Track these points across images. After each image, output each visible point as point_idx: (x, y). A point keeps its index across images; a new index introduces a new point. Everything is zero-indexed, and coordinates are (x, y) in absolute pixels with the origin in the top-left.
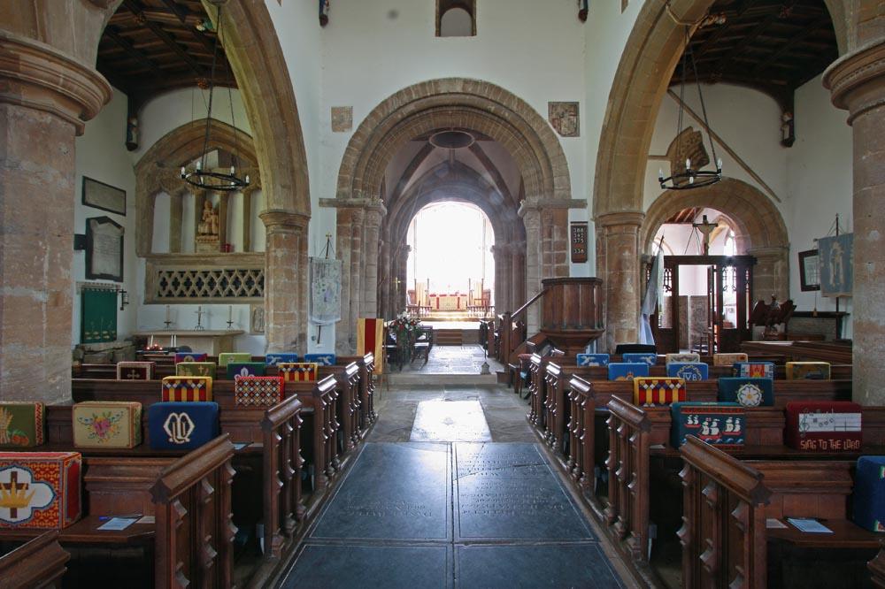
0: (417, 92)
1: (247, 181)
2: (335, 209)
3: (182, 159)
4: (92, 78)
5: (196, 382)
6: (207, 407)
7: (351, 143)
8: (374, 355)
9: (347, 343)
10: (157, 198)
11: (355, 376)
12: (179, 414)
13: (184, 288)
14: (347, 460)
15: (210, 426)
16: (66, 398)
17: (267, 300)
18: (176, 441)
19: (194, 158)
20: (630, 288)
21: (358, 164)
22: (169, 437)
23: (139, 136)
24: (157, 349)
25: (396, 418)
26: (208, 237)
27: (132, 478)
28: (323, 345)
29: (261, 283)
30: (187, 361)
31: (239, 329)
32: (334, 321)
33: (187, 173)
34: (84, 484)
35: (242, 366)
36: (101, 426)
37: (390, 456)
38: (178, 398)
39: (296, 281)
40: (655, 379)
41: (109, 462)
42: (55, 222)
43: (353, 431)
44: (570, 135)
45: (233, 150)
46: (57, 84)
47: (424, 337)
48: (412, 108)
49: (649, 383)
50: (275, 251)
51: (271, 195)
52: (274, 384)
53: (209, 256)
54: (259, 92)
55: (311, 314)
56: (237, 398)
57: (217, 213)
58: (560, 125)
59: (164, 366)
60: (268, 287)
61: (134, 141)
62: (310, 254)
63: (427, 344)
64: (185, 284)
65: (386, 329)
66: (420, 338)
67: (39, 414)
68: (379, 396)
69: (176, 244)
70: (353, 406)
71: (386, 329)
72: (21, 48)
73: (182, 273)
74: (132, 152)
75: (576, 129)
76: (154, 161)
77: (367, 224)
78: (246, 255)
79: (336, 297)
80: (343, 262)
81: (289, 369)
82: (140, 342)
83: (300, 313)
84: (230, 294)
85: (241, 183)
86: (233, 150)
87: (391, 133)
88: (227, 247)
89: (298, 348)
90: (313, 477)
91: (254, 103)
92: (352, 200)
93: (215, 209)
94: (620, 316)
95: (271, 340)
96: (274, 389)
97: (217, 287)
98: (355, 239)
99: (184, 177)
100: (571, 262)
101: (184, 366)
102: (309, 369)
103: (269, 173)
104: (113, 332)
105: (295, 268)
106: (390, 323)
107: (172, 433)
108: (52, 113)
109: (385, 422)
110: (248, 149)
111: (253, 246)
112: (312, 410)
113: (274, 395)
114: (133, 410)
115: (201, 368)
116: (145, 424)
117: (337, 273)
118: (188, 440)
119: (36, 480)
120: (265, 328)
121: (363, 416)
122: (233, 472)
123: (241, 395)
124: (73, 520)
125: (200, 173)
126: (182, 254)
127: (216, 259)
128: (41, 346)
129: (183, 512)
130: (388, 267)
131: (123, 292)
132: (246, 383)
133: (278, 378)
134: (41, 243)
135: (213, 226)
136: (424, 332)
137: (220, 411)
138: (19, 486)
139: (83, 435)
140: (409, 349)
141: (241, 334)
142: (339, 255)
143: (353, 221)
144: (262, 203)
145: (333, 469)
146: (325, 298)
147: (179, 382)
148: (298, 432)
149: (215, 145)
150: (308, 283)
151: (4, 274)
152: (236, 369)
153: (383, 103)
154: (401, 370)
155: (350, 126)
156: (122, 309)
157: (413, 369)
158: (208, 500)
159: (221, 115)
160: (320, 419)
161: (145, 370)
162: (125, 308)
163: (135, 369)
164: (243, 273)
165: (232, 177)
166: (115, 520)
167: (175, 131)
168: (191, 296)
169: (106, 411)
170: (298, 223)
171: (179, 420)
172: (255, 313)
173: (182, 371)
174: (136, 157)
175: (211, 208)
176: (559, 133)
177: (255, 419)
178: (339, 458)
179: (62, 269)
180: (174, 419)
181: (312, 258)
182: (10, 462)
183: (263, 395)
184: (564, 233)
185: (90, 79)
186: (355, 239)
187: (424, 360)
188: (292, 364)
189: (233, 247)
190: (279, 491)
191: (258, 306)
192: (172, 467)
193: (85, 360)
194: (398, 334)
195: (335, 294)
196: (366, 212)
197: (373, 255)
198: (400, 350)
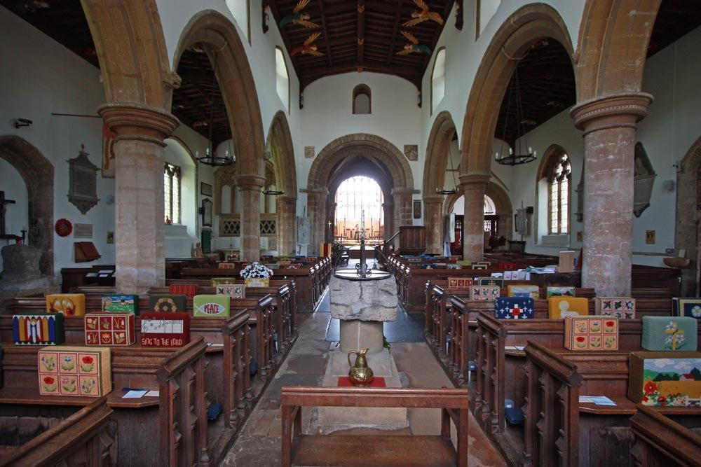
7: (314, 163)
20: (437, 231)
44: (414, 160)
48: (342, 147)
94: (432, 243)
100: (213, 185)
142: (308, 215)
155: (313, 155)
184: (411, 204)
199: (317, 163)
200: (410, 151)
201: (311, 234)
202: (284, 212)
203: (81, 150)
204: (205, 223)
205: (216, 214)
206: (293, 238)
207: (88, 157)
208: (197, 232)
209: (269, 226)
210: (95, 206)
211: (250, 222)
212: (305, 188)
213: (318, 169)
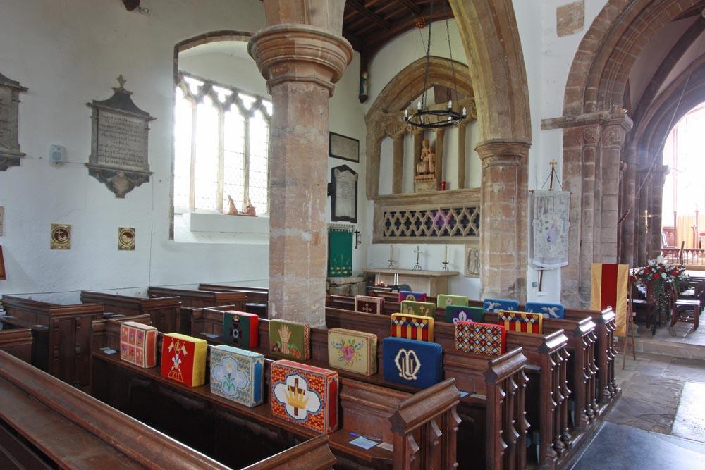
1: (464, 114)
2: (562, 129)
3: (403, 103)
4: (340, 44)
5: (420, 321)
6: (428, 346)
7: (582, 45)
8: (614, 310)
9: (576, 292)
10: (383, 143)
11: (590, 335)
12: (407, 351)
14: (579, 437)
15: (435, 370)
16: (321, 324)
17: (483, 239)
18: (405, 377)
19: (413, 99)
21: (591, 70)
22: (399, 371)
23: (368, 88)
24: (382, 286)
25: (648, 397)
26: (425, 176)
27: (375, 404)
28: (547, 292)
29: (476, 221)
30: (409, 299)
31: (453, 270)
32: (559, 265)
33: (408, 115)
34: (340, 400)
35: (460, 310)
36: (348, 352)
37: (641, 448)
38: (404, 335)
39: (514, 219)
41: (357, 385)
42: (316, 173)
43: (587, 403)
45: (449, 84)
46: (317, 57)
47: (691, 292)
50: (491, 186)
51: (488, 124)
52: (495, 332)
53: (426, 195)
54: (475, 14)
55: (532, 256)
56: (457, 343)
57: (433, 152)
59: (391, 304)
60: (483, 227)
61: (365, 93)
62: (531, 185)
63: (698, 302)
64: (405, 224)
65: (631, 279)
66: (685, 293)
67: (306, 333)
68: (621, 364)
69: (398, 185)
70: (588, 373)
71: (631, 279)
72: (296, 34)
73: (403, 213)
74: (364, 104)
76: (380, 108)
77: (605, 143)
78: (461, 192)
79: (562, 237)
80: (571, 193)
81: (510, 318)
82: (370, 278)
83: (519, 255)
84: (446, 233)
85: (458, 116)
86: (449, 84)
87: (640, 18)
88: (443, 185)
89: (516, 295)
90: (538, 447)
91: (470, 28)
92: (583, 116)
93: (432, 147)
95: (487, 284)
96: (495, 338)
97: (434, 226)
98: (588, 164)
99: (406, 119)
101: (407, 303)
102: (532, 320)
103: (485, 100)
104: (350, 268)
105: (513, 204)
106: (637, 270)
107: (401, 368)
108: (314, 82)
109: (632, 400)
110: (463, 79)
111: (468, 181)
112: (538, 368)
113: (495, 344)
114: (371, 341)
115: (422, 308)
116: (380, 356)
117: (563, 208)
118: (415, 378)
119: (310, 389)
120: (480, 270)
121: (601, 389)
122: (459, 421)
123: (461, 340)
124: (332, 429)
125: (420, 113)
126: (403, 194)
127: (434, 198)
128: (307, 278)
129: (416, 448)
130: (633, 197)
131: (357, 232)
132: (466, 329)
133: (499, 327)
134: (307, 192)
135: (430, 164)
136: (693, 285)
137: (444, 353)
138: (300, 391)
139: (334, 355)
140: (667, 306)
141: (454, 275)
142: (566, 186)
143: (585, 142)
144: (478, 134)
145: (562, 444)
146: (549, 238)
147: (404, 320)
148: (524, 390)
149: (432, 83)
150: (528, 220)
151: (286, 219)
152: (455, 312)
154: (654, 334)
155: (581, 24)
156: (356, 247)
157: (673, 334)
158: (436, 443)
159: (439, 51)
160: (547, 380)
161: (376, 304)
162: (358, 246)
163: (369, 303)
164: (458, 211)
165: (449, 112)
166: (361, 438)
167: (396, 77)
168: (411, 235)
169: (352, 338)
170: (516, 152)
171: (407, 357)
172: (470, 254)
173: (405, 309)
174: (367, 107)
175: (428, 146)
177: (477, 367)
178: (570, 432)
179: (320, 212)
180: (403, 355)
181: (533, 191)
182: (294, 370)
183: (483, 343)
185: (339, 46)
186: (588, 164)
187: (692, 325)
188: (512, 312)
189: (449, 184)
190: (503, 453)
191: (473, 246)
192: (407, 401)
193: (331, 291)
194: (649, 286)
195: (561, 233)
196: (604, 129)
197: (612, 183)
198: (653, 307)
199: (594, 41)
201: (572, 237)
203: (118, 86)
204: (339, 213)
205: (369, 198)
206: (519, 248)
207: (132, 97)
210: (144, 185)
211: (284, 186)
212: (559, 114)
213: (595, 60)
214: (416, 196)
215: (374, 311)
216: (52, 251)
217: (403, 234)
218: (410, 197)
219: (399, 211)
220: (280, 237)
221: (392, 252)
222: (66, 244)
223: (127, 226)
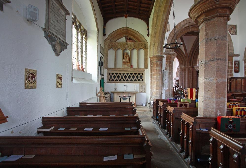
0: (189, 20)
13: (121, 78)
40: (233, 103)
44: (234, 35)
48: (187, 25)
49: (239, 109)
53: (127, 69)
58: (231, 31)
73: (116, 74)
75: (236, 33)
81: (232, 104)
110: (137, 36)
127: (128, 70)
147: (241, 109)
153: (179, 23)
155: (169, 30)
161: (187, 104)
163: (184, 104)
164: (135, 74)
176: (231, 34)
184: (232, 64)
200: (232, 29)
202: (157, 66)
208: (98, 79)
209: (139, 76)
213: (172, 40)
214: (122, 69)
215: (186, 107)
216: (25, 89)
217: (117, 80)
218: (121, 69)
219: (111, 73)
220: (223, 82)
221: (115, 86)
222: (34, 85)
223: (60, 74)
